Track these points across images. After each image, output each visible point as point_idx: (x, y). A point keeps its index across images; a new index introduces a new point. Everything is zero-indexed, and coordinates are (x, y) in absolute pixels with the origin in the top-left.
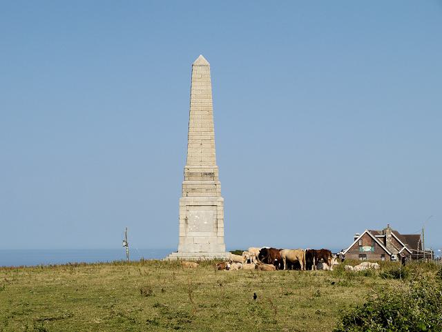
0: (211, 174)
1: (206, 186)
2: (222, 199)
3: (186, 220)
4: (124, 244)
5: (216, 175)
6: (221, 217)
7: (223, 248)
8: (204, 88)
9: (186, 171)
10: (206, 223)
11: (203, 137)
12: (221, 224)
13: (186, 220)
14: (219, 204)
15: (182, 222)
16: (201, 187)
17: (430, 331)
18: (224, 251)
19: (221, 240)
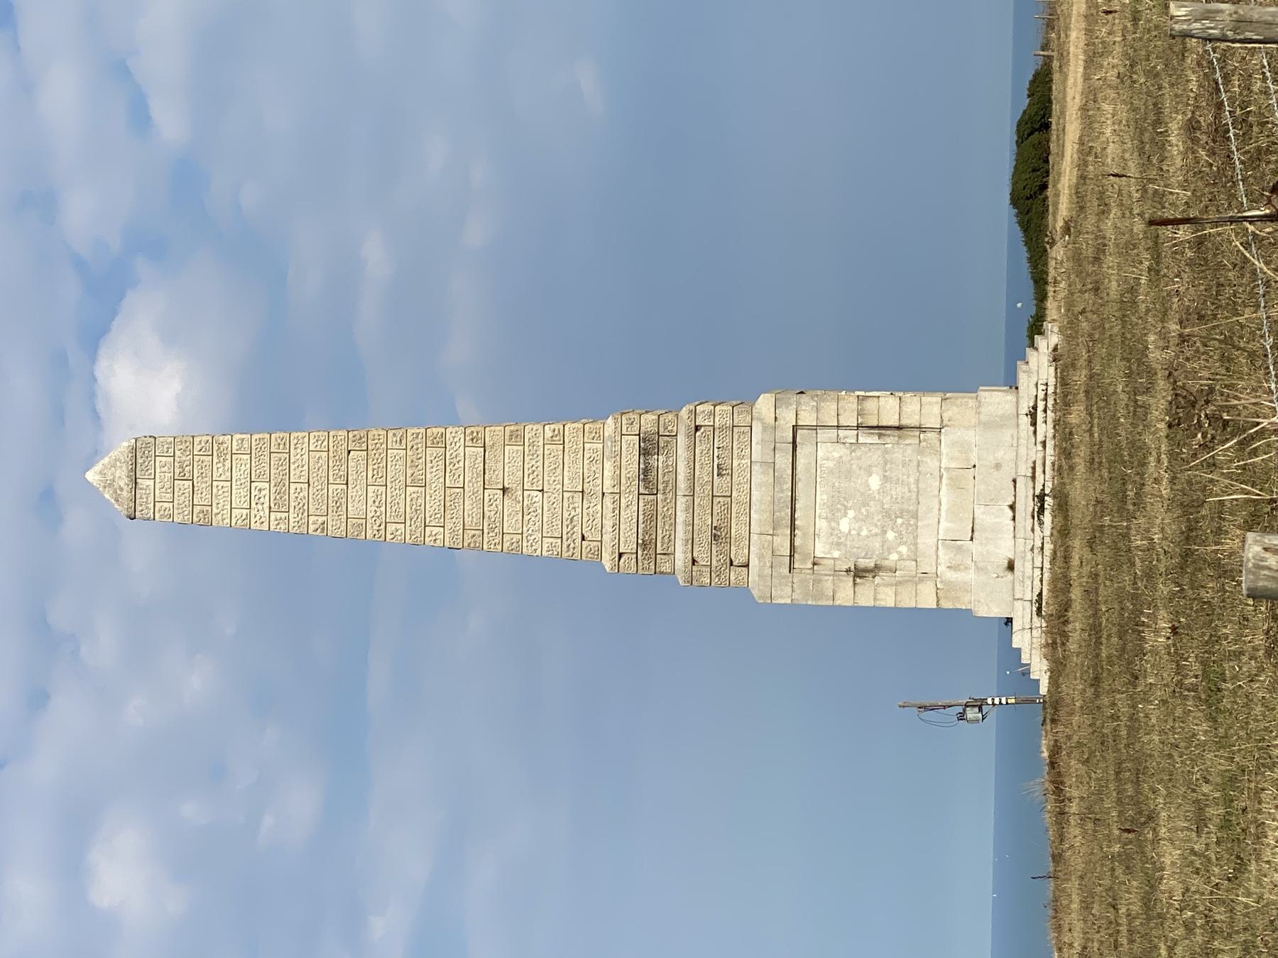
0: (649, 447)
1: (702, 475)
2: (765, 404)
3: (859, 573)
4: (972, 714)
5: (648, 421)
6: (847, 407)
7: (996, 401)
8: (240, 473)
9: (628, 564)
10: (875, 482)
11: (474, 486)
12: (887, 408)
13: (859, 573)
14: (788, 418)
15: (867, 595)
16: (701, 500)
17: (1277, 867)
18: (1010, 397)
19: (960, 408)
